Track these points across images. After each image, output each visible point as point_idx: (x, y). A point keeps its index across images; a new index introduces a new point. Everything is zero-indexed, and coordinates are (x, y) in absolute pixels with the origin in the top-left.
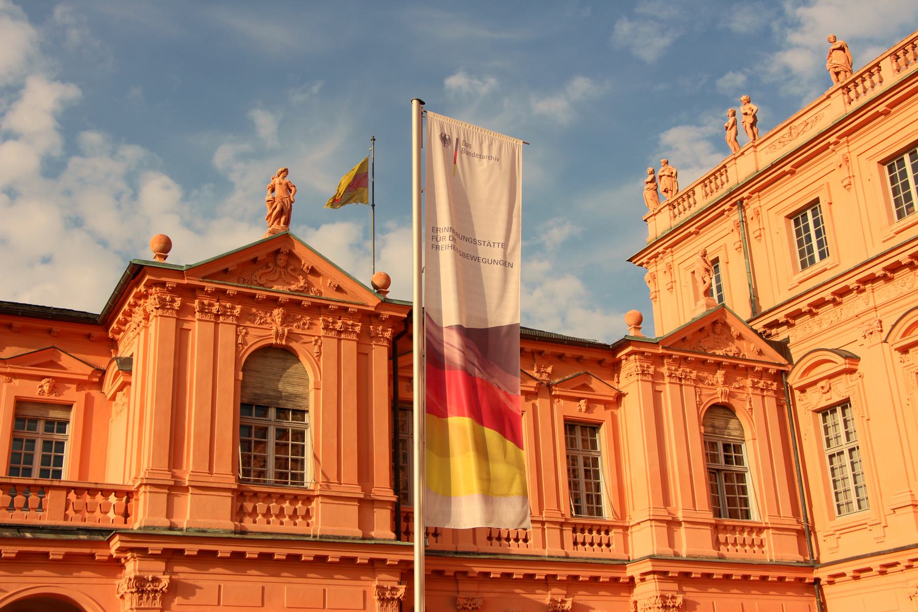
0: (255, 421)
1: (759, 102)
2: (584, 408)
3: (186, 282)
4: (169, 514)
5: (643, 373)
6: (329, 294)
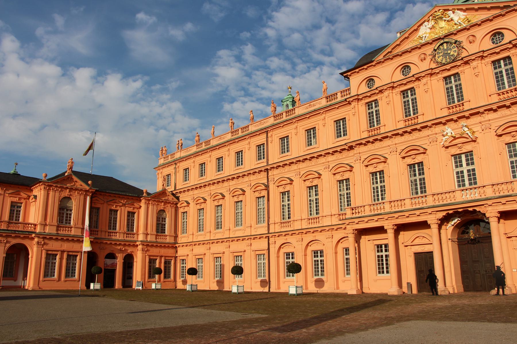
0: (62, 212)
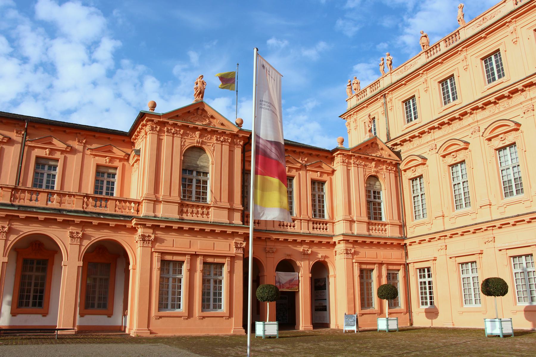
0: (188, 176)
1: (393, 56)
2: (319, 175)
3: (161, 120)
4: (154, 211)
5: (343, 162)
6: (218, 126)
